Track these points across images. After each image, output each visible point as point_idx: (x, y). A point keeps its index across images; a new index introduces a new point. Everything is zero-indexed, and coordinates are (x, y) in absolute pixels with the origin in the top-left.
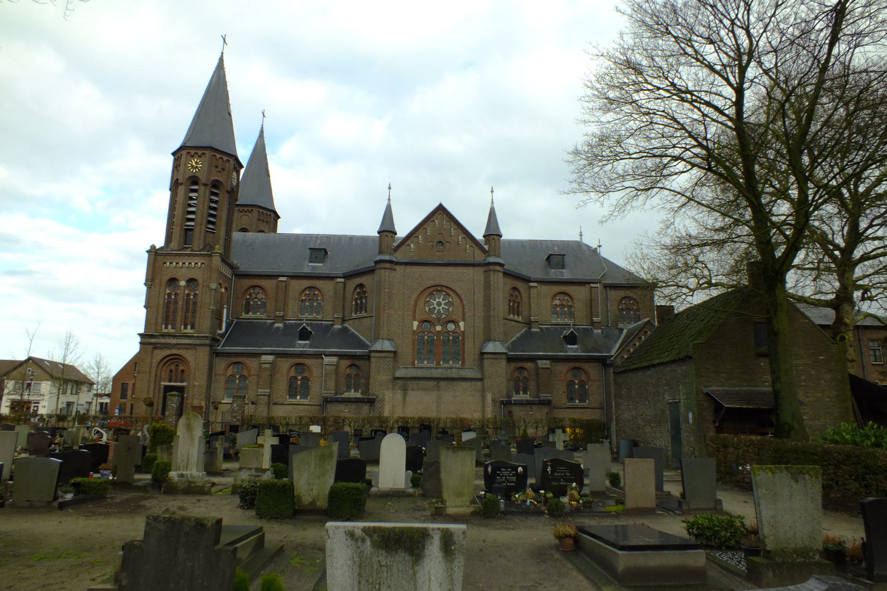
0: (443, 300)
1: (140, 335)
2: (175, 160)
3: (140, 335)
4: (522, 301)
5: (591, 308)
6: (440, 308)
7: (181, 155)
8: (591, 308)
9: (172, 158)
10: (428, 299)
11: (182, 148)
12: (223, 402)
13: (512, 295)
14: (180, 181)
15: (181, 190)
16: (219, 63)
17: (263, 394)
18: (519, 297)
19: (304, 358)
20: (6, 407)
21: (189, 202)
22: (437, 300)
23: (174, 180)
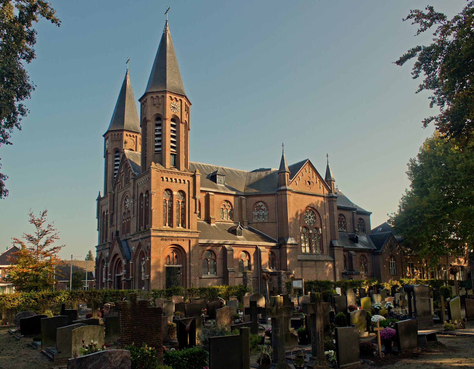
0: (311, 215)
1: (96, 247)
2: (142, 105)
3: (96, 247)
4: (345, 221)
5: (148, 286)
6: (310, 220)
7: (146, 99)
8: (148, 286)
9: (103, 138)
10: (311, 211)
11: (108, 132)
12: (203, 277)
13: (339, 218)
14: (109, 152)
15: (110, 157)
16: (163, 34)
17: (232, 271)
18: (344, 219)
19: (248, 247)
20: (422, 122)
21: (115, 168)
22: (309, 215)
23: (143, 119)
